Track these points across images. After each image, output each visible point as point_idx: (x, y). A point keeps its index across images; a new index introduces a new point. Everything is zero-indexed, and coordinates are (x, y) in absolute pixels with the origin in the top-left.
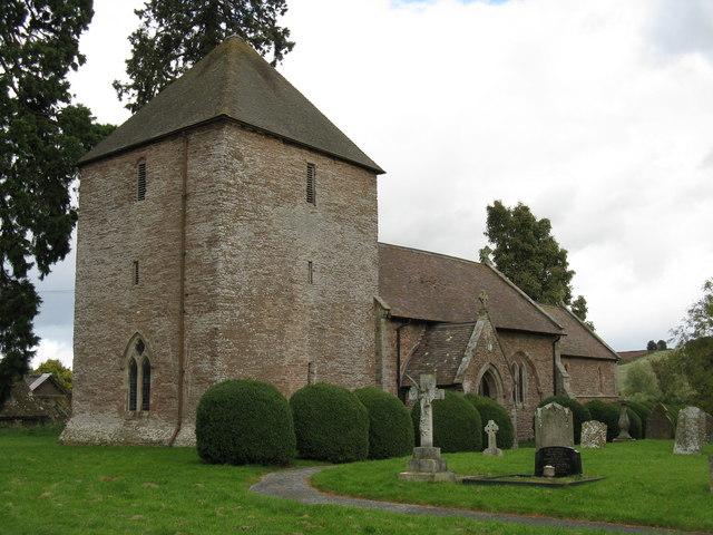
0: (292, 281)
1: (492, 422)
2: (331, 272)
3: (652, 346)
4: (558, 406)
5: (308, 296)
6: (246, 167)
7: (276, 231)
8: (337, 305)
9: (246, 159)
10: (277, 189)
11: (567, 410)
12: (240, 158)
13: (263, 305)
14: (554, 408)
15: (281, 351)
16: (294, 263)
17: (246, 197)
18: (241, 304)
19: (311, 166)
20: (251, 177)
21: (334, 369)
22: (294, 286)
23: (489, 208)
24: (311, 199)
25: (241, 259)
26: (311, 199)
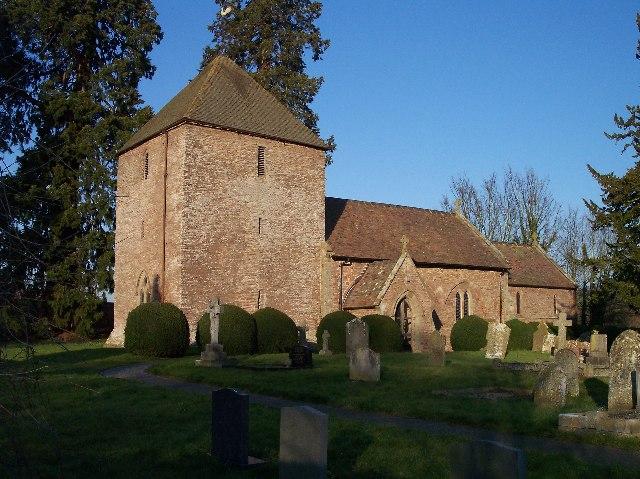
19: (261, 149)
24: (261, 171)
26: (261, 171)
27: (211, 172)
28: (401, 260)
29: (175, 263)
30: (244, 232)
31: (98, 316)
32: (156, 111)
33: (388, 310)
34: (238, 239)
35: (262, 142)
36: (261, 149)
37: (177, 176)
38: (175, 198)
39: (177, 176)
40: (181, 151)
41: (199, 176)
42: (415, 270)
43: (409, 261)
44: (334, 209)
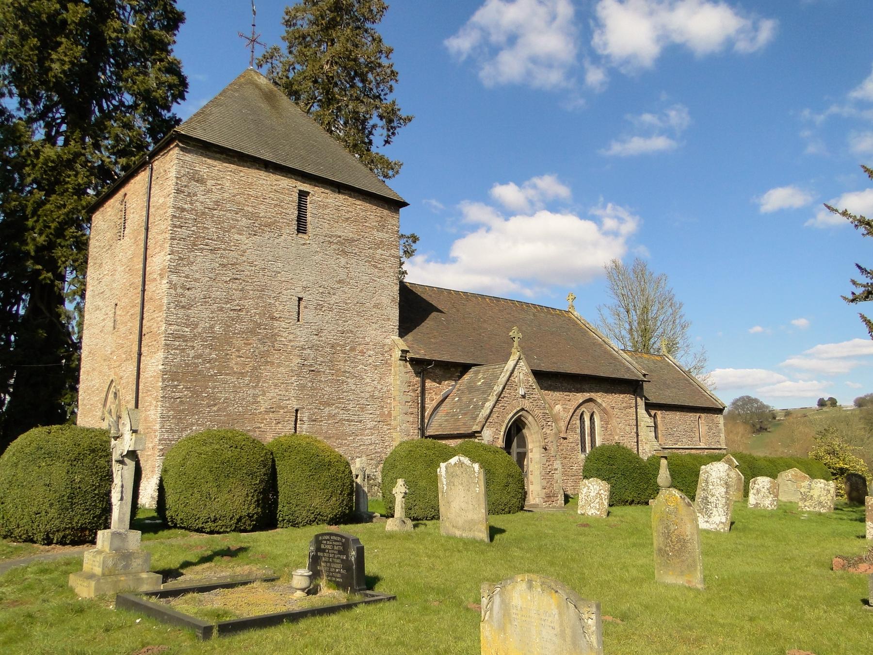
0: (273, 318)
1: (400, 482)
2: (331, 310)
3: (822, 403)
4: (466, 460)
5: (295, 335)
6: (210, 191)
7: (251, 264)
8: (338, 345)
9: (210, 183)
10: (254, 216)
11: (476, 466)
12: (201, 181)
13: (230, 344)
14: (461, 464)
15: (255, 396)
16: (276, 298)
17: (209, 224)
18: (197, 344)
19: (303, 195)
20: (217, 203)
21: (331, 416)
22: (276, 324)
23: (183, 13)
24: (301, 227)
25: (197, 293)
26: (301, 227)
27: (219, 222)
28: (511, 363)
29: (154, 363)
30: (275, 319)
31: (486, 50)
32: (184, 119)
33: (495, 439)
34: (264, 331)
35: (306, 187)
36: (303, 195)
37: (161, 228)
38: (159, 260)
39: (161, 228)
40: (170, 185)
41: (195, 230)
42: (537, 392)
43: (523, 373)
44: (414, 308)
